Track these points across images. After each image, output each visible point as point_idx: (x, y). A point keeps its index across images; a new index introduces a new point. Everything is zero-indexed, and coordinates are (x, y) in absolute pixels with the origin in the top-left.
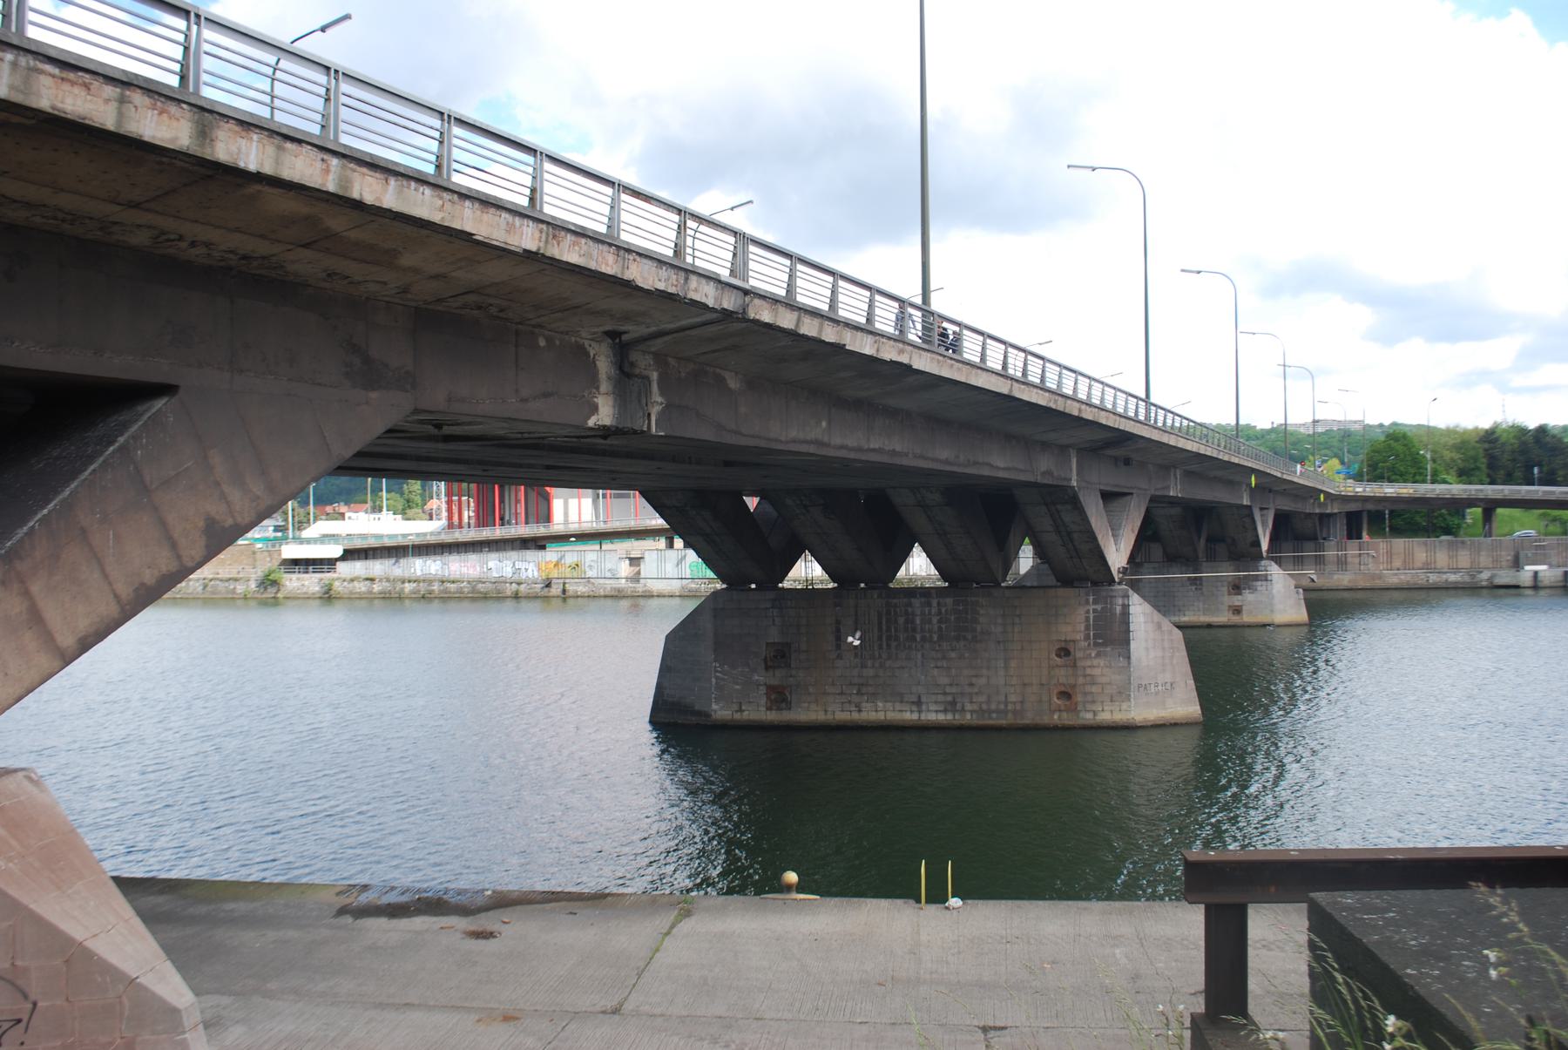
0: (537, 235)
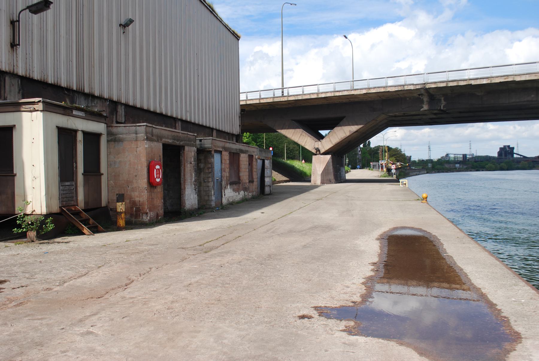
0: (366, 91)
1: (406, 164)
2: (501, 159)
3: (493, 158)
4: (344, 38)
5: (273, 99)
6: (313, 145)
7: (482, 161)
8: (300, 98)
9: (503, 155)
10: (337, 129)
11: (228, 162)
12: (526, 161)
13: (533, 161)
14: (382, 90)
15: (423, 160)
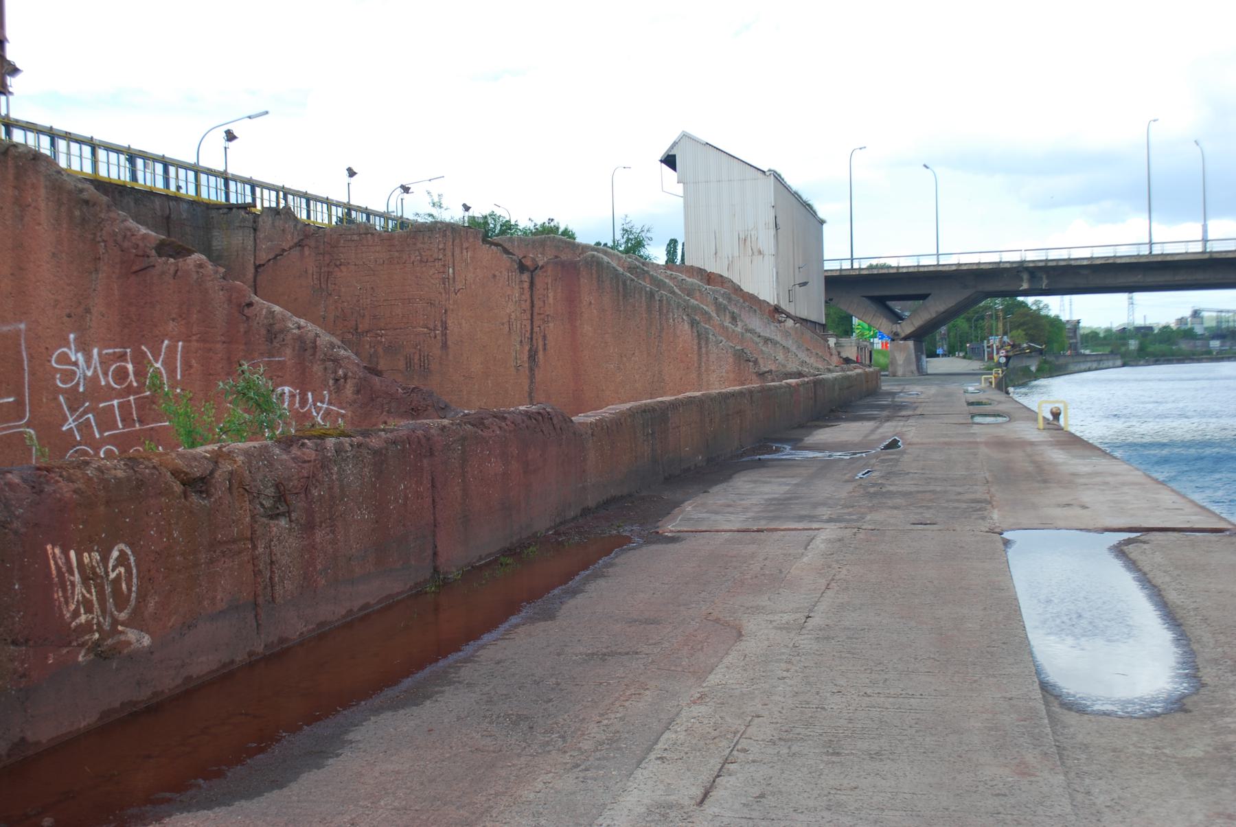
1: (135, 426)
4: (925, 168)
14: (975, 267)
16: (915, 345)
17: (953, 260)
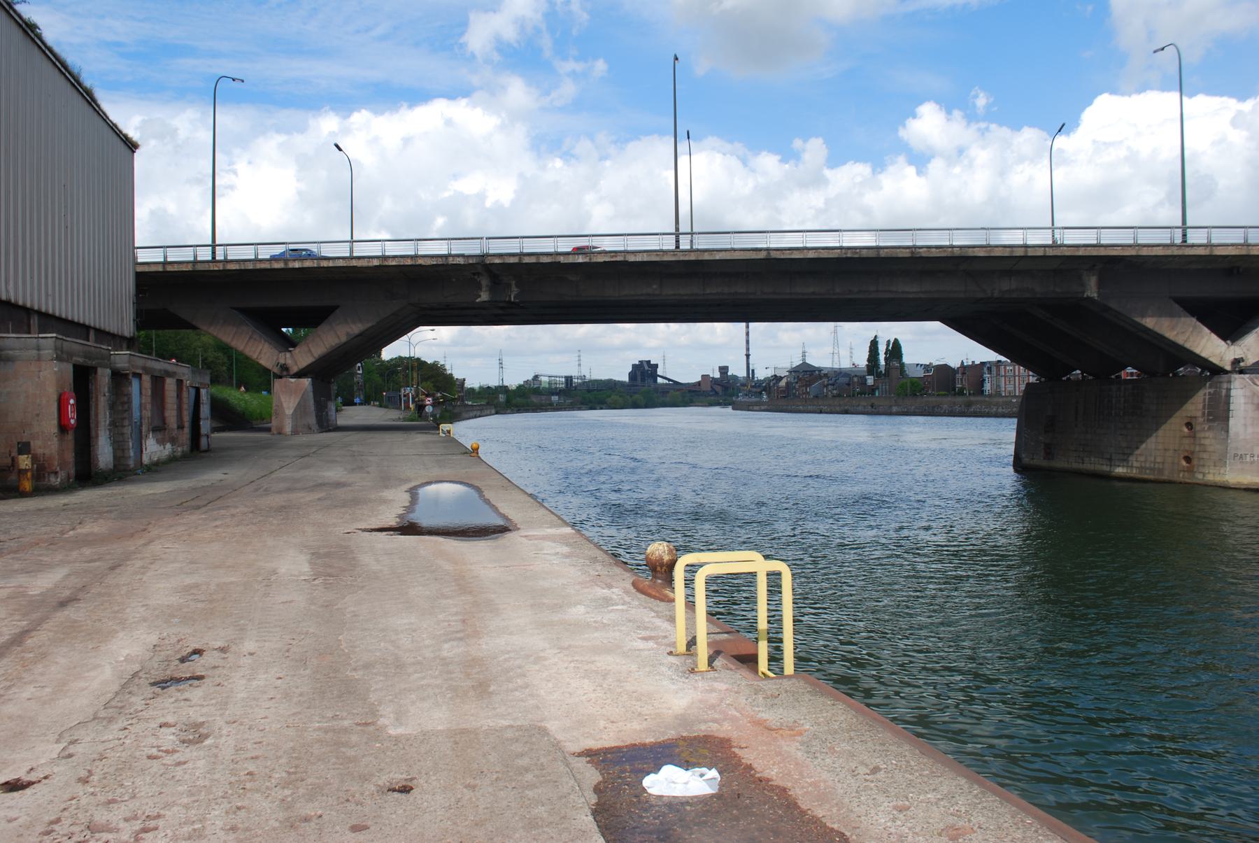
2: (634, 386)
3: (622, 383)
5: (194, 266)
6: (275, 358)
7: (600, 390)
8: (250, 266)
9: (639, 378)
10: (323, 328)
11: (149, 393)
12: (678, 390)
13: (690, 391)
14: (409, 262)
15: (489, 387)
16: (314, 384)
17: (374, 250)
